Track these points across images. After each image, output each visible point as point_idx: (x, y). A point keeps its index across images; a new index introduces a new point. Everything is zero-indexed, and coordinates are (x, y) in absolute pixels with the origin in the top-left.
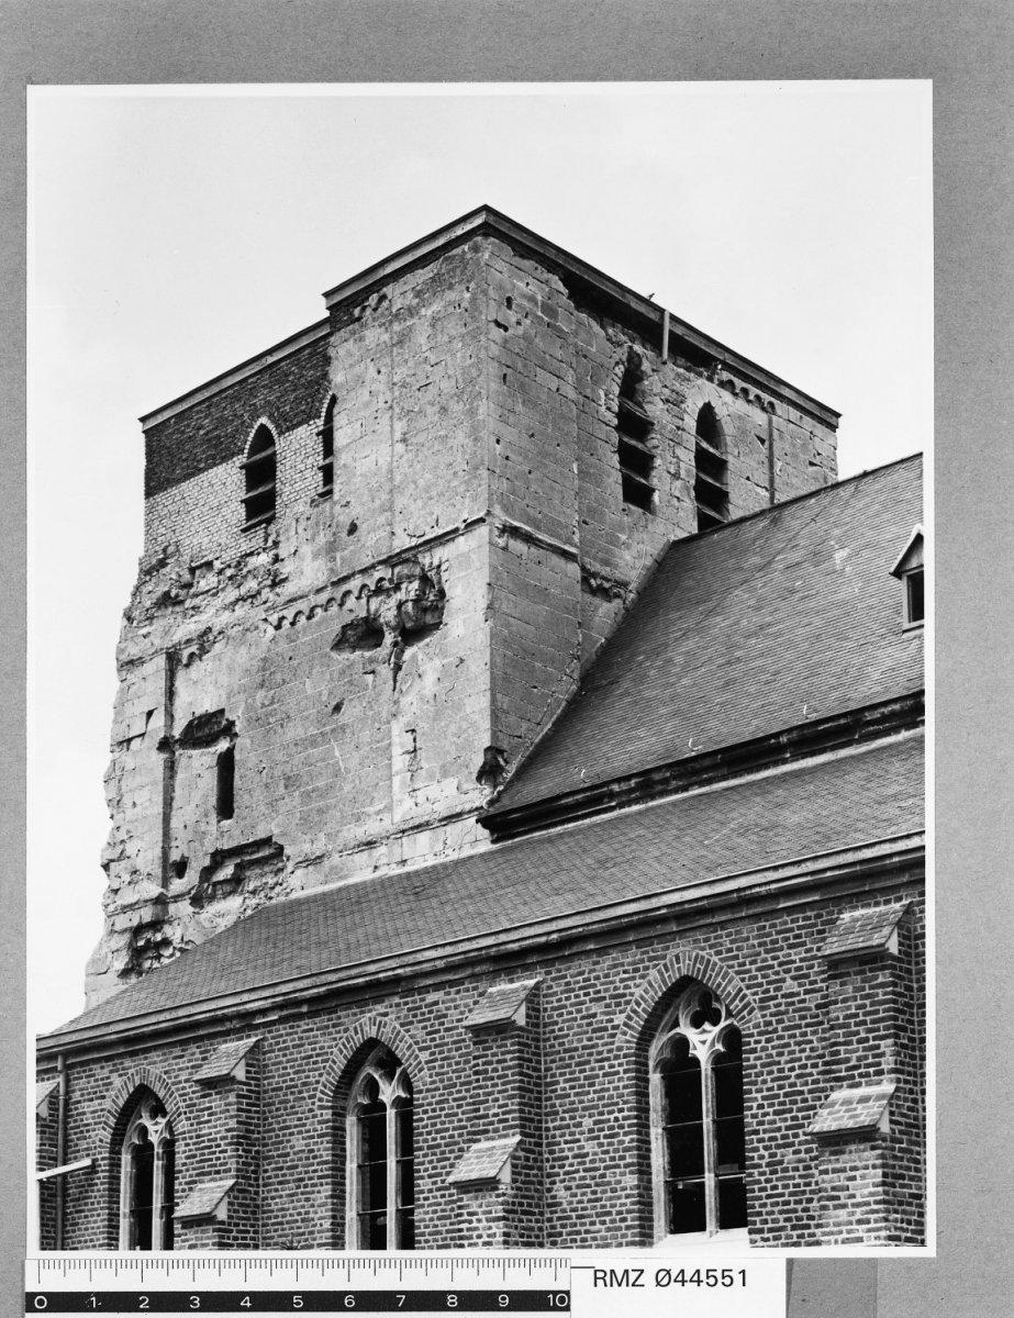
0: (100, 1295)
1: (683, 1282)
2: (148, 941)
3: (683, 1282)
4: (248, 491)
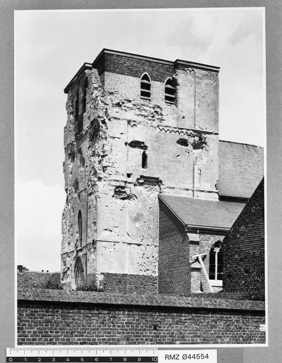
0: (27, 358)
1: (190, 358)
2: (119, 190)
3: (190, 358)
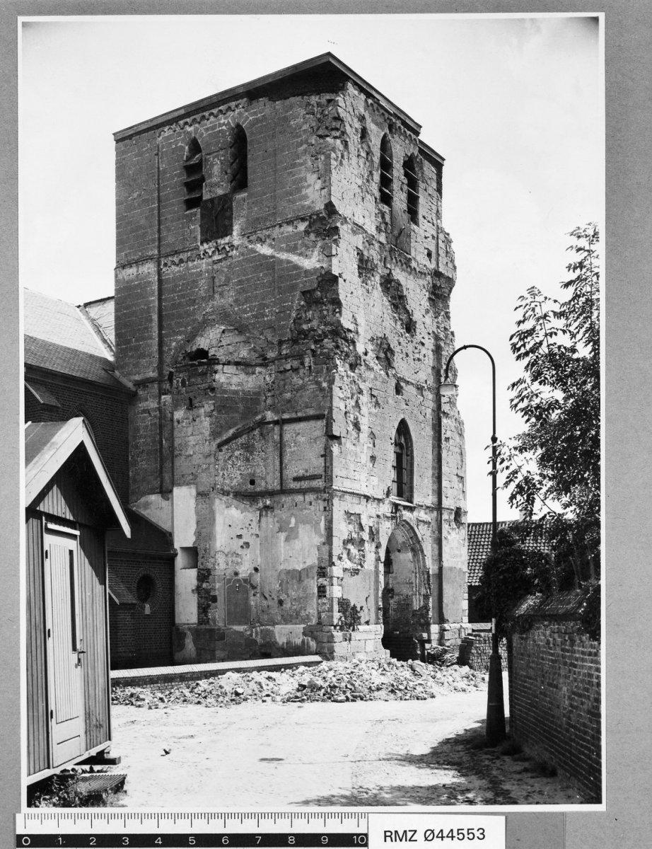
0: (64, 837)
1: (442, 837)
3: (442, 837)
4: (29, 340)
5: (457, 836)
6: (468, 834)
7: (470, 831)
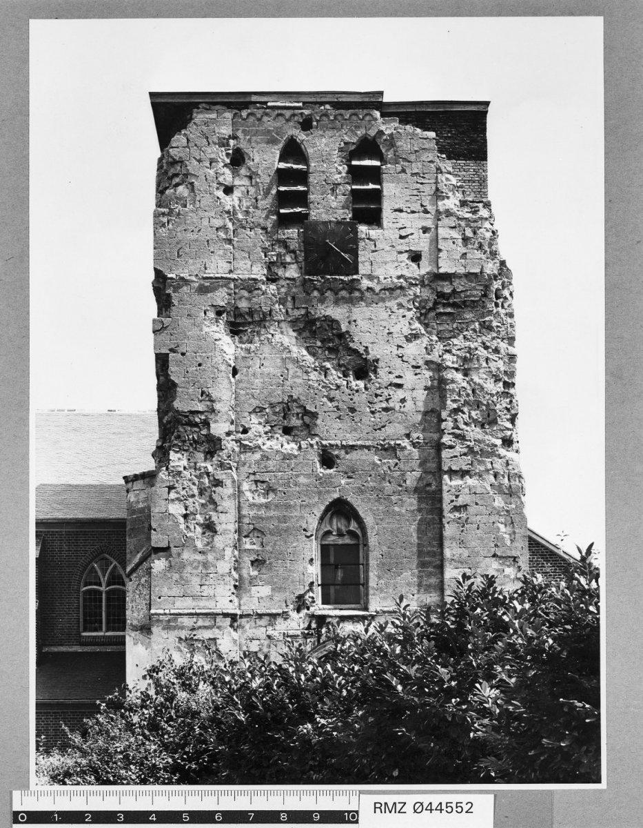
0: (60, 813)
1: (431, 810)
3: (431, 810)
5: (445, 809)
6: (457, 807)
7: (458, 805)
